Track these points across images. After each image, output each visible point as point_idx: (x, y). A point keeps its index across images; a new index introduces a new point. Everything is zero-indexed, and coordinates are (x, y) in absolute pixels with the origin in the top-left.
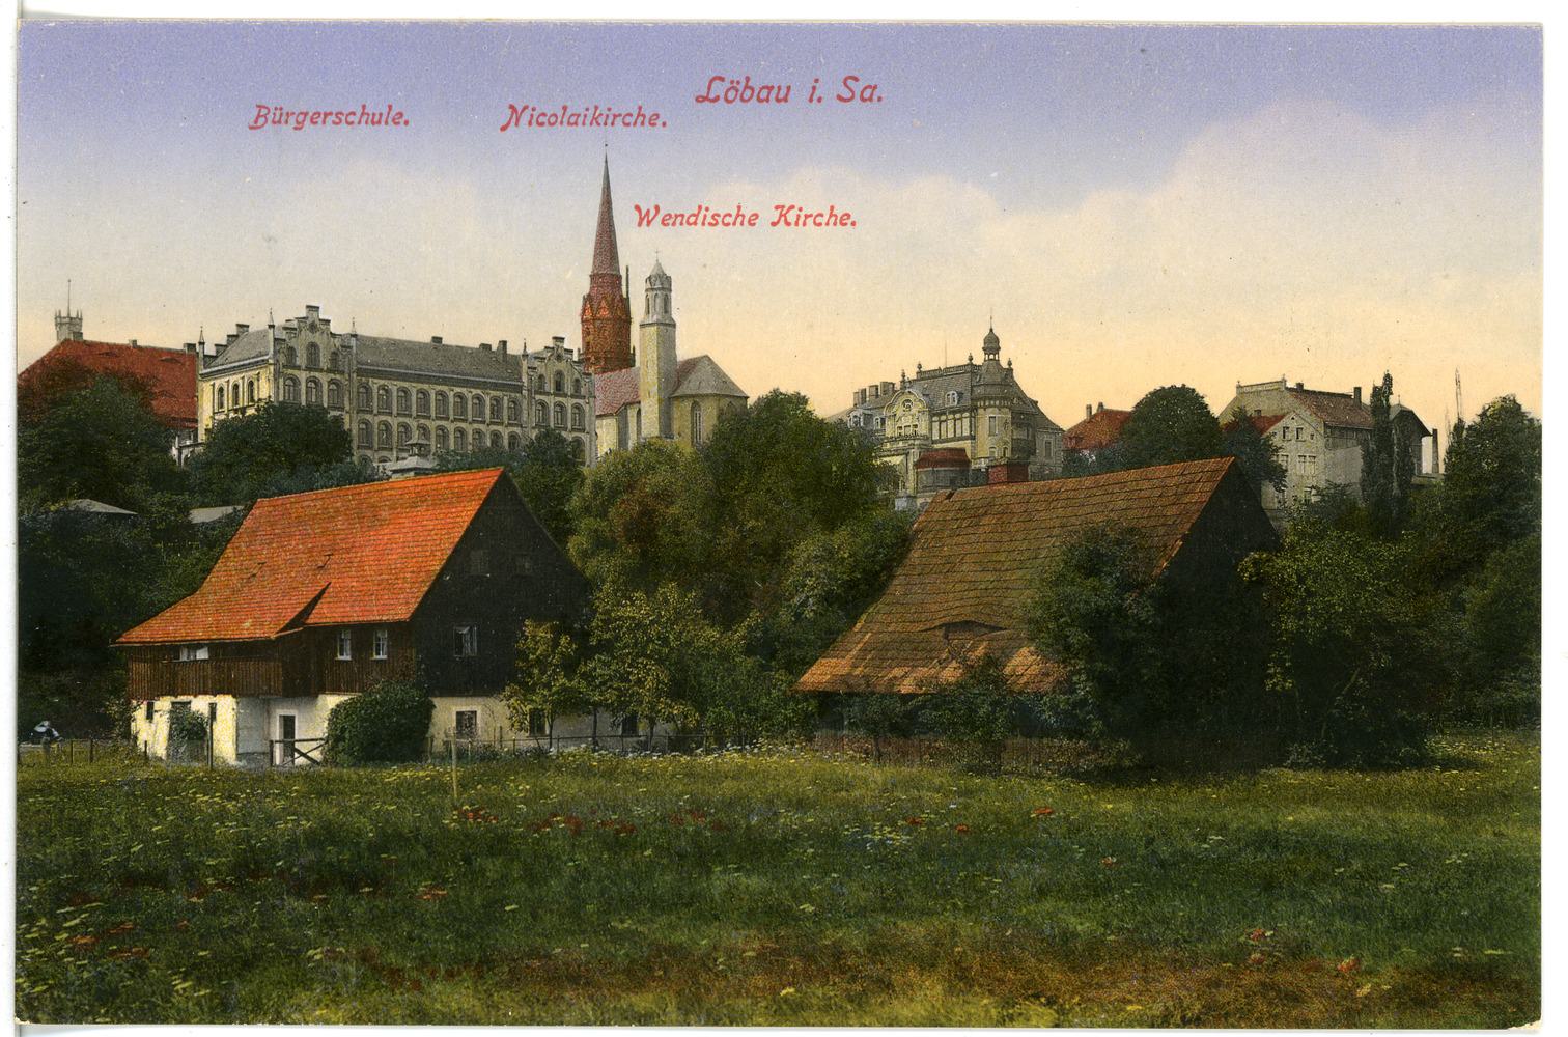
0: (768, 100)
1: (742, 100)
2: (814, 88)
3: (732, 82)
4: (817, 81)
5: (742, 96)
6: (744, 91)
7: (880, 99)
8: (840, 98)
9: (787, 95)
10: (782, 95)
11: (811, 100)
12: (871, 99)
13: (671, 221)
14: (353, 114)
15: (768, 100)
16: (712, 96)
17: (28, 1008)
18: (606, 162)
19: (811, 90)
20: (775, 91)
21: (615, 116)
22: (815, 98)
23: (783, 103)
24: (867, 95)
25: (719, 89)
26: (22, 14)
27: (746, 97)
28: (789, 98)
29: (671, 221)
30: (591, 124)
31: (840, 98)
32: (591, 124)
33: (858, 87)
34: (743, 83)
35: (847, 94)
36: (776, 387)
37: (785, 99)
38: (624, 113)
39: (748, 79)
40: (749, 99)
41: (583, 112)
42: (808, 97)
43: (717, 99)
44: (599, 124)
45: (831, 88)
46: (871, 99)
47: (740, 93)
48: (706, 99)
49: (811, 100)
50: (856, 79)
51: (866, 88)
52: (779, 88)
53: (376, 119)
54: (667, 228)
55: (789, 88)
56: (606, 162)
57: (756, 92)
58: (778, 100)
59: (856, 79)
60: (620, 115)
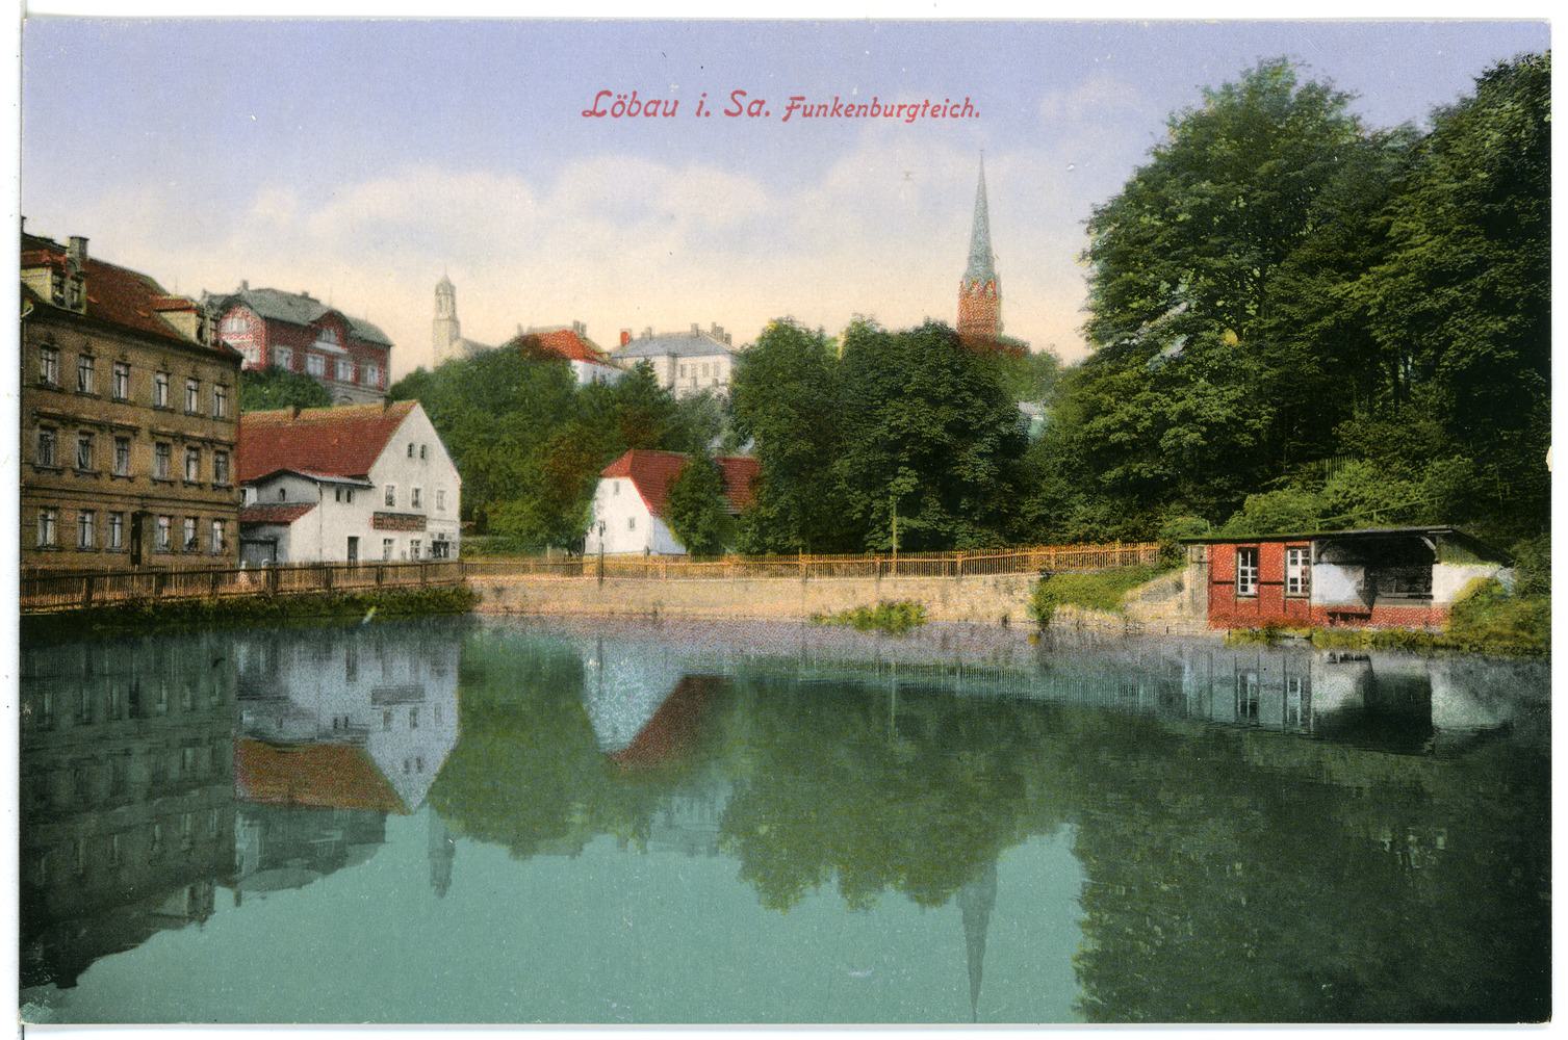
0: (655, 114)
1: (630, 114)
2: (702, 103)
3: (619, 96)
4: (704, 95)
5: (629, 111)
6: (628, 106)
7: (767, 114)
8: (727, 113)
9: (674, 110)
10: (669, 109)
11: (698, 114)
12: (758, 113)
13: (853, 113)
14: (958, 106)
15: (655, 114)
16: (599, 110)
19: (699, 104)
20: (662, 106)
21: (901, 107)
22: (703, 113)
23: (755, 116)
24: (754, 109)
25: (606, 103)
26: (26, 15)
27: (650, 110)
28: (677, 112)
29: (853, 113)
30: (832, 115)
31: (727, 113)
32: (832, 115)
33: (745, 102)
34: (630, 96)
35: (735, 109)
36: (388, 838)
37: (673, 114)
38: (909, 104)
39: (635, 93)
40: (620, 115)
41: (943, 104)
42: (679, 106)
43: (604, 113)
44: (839, 115)
45: (720, 101)
46: (758, 113)
47: (627, 108)
48: (593, 113)
49: (698, 114)
50: (744, 93)
51: (752, 103)
52: (667, 103)
53: (863, 110)
54: (850, 119)
55: (676, 103)
57: (642, 111)
58: (665, 114)
59: (744, 93)
60: (905, 106)
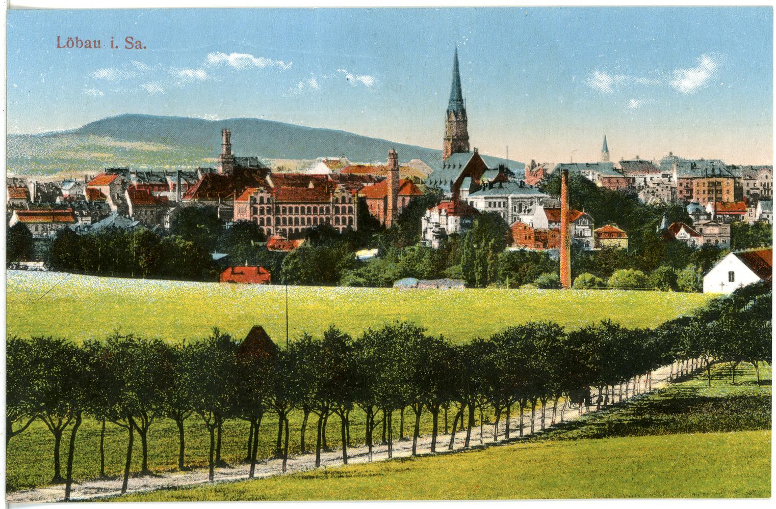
6: (73, 42)
17: (769, 10)
18: (457, 69)
56: (457, 69)
